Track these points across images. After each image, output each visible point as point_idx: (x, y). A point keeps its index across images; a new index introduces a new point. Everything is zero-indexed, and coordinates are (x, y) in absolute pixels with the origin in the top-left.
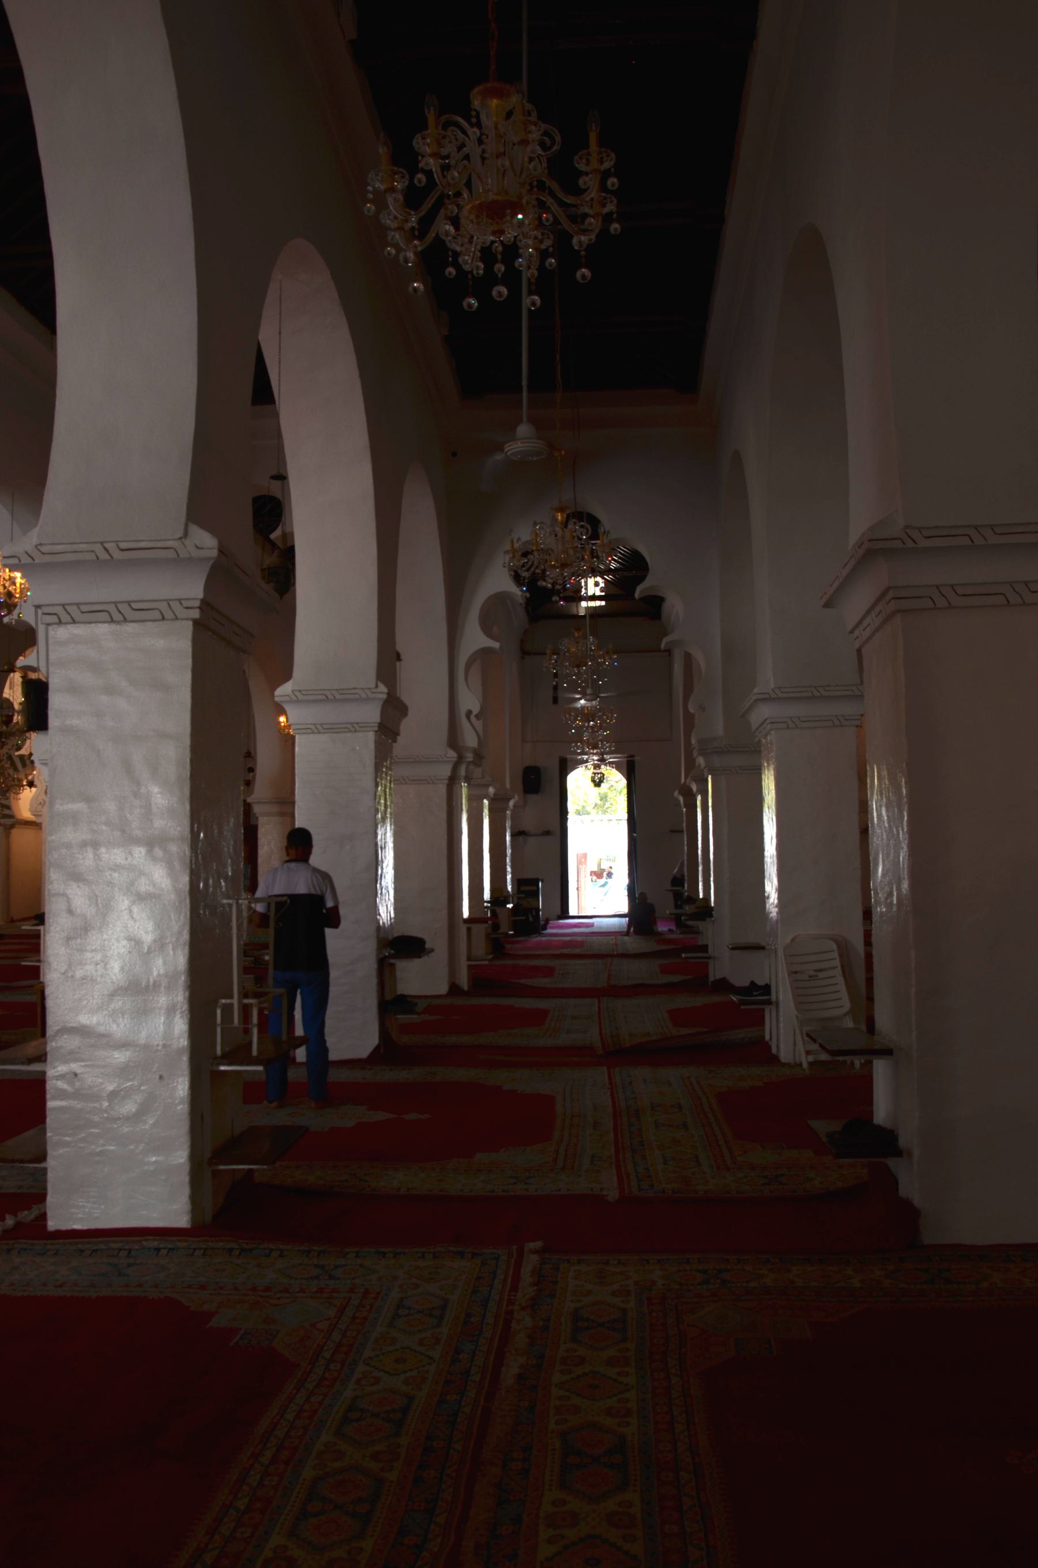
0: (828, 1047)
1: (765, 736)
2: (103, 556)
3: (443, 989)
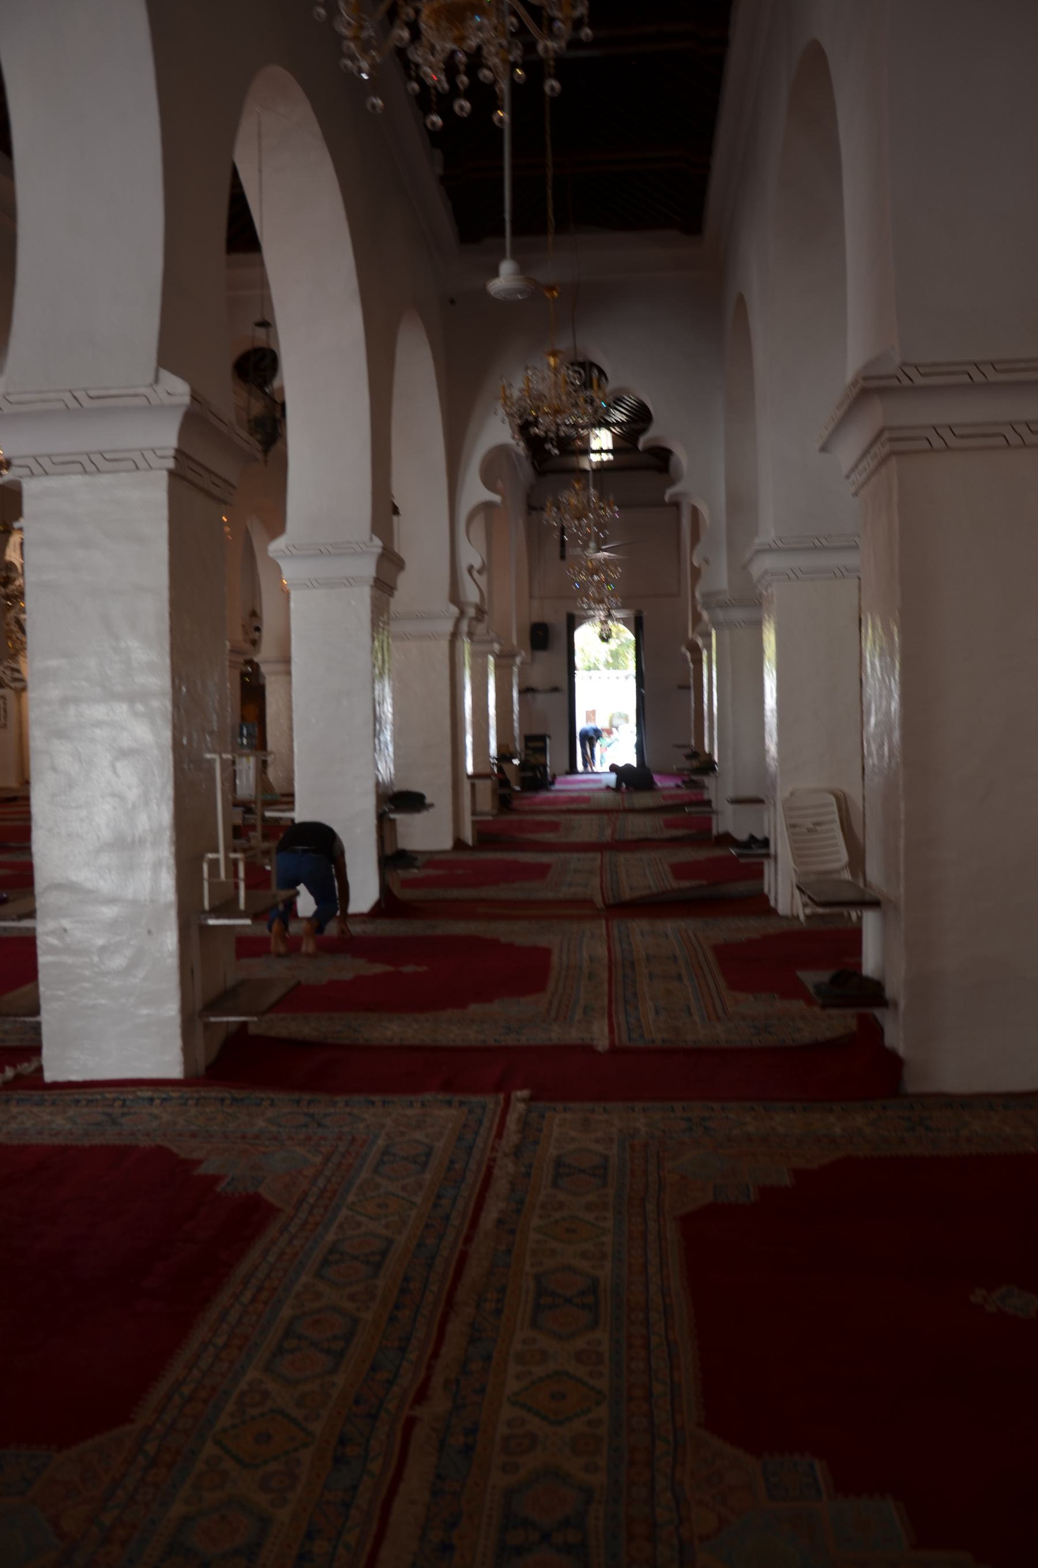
0: (815, 898)
1: (766, 589)
2: (72, 404)
3: (447, 844)
